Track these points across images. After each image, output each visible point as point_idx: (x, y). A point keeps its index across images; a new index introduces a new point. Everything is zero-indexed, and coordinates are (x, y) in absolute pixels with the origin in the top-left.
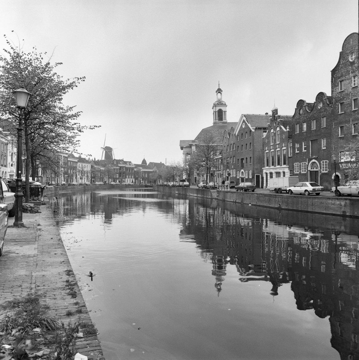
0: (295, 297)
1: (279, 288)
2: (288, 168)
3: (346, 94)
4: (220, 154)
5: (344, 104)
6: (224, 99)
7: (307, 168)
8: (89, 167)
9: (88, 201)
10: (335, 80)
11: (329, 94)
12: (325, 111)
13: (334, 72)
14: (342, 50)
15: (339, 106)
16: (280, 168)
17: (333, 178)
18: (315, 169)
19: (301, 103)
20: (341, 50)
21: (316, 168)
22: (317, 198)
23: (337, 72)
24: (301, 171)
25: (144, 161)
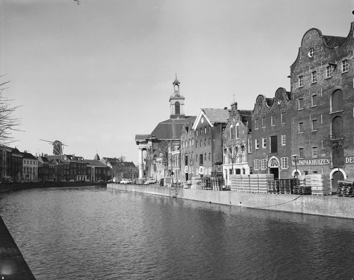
12: (284, 107)
13: (293, 67)
21: (276, 165)
23: (296, 67)
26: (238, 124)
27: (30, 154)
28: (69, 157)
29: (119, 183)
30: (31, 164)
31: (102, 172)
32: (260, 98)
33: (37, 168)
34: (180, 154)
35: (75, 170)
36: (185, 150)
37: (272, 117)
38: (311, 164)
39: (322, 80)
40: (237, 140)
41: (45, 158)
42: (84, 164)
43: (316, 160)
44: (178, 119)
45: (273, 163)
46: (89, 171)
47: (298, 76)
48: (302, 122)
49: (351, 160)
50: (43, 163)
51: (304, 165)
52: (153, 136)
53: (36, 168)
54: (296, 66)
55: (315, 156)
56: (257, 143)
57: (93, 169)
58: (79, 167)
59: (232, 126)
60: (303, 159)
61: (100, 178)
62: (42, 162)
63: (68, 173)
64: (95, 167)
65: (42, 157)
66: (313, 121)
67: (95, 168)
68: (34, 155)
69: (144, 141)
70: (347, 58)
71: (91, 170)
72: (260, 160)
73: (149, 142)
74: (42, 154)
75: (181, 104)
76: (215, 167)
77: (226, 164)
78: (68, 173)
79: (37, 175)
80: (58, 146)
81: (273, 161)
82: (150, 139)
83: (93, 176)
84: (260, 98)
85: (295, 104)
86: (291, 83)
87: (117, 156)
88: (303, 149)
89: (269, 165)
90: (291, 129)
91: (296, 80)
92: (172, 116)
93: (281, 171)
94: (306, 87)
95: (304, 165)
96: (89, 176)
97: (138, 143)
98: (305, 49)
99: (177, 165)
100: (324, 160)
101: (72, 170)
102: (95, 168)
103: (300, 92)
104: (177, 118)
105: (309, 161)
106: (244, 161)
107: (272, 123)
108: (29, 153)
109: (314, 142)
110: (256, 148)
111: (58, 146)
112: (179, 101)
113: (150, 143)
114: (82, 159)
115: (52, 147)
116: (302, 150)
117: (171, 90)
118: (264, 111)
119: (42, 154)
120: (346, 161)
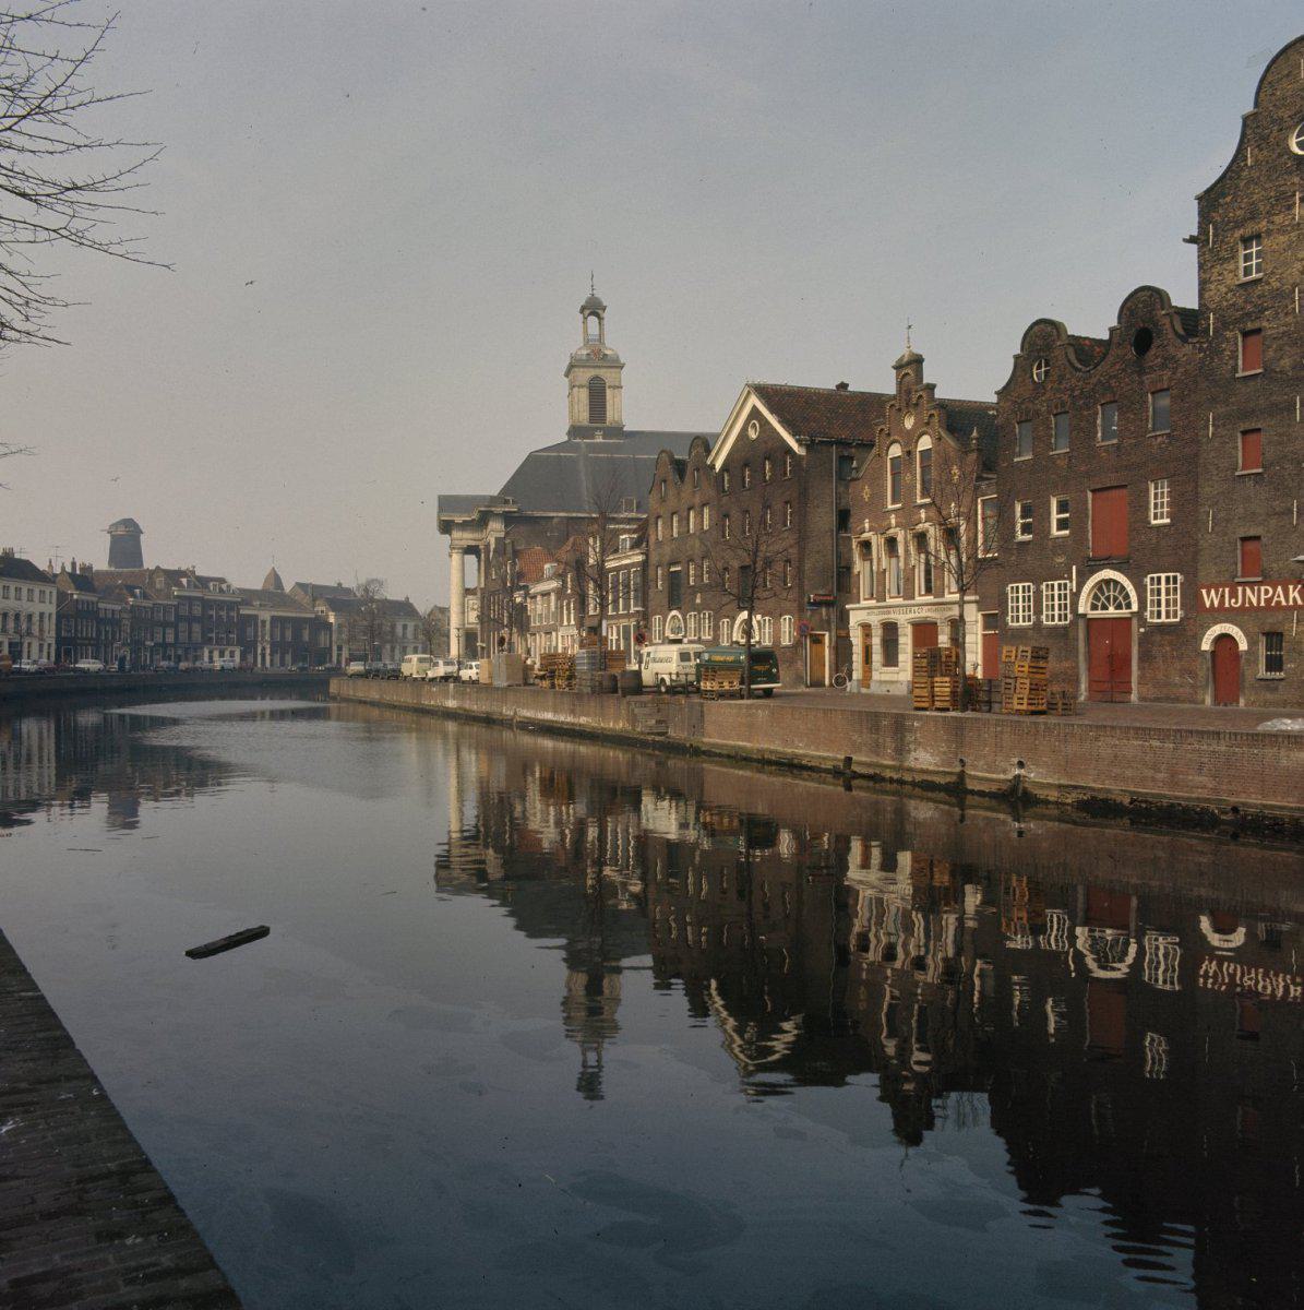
0: (1194, 1262)
1: (1193, 1271)
3: (1271, 291)
4: (636, 545)
5: (1263, 333)
6: (612, 345)
7: (1075, 604)
8: (47, 596)
10: (1215, 235)
11: (1185, 296)
12: (1163, 366)
13: (1209, 201)
14: (1256, 104)
15: (1236, 344)
16: (879, 607)
17: (1206, 645)
18: (1111, 609)
20: (1249, 108)
21: (1119, 607)
23: (1228, 199)
24: (1044, 617)
25: (275, 578)
26: (925, 443)
27: (28, 563)
28: (173, 576)
30: (30, 600)
31: (297, 635)
32: (1043, 340)
33: (54, 617)
34: (645, 565)
35: (197, 628)
36: (667, 550)
37: (1099, 407)
40: (921, 506)
41: (83, 579)
42: (232, 606)
44: (599, 440)
45: (1103, 599)
46: (250, 631)
47: (1238, 233)
48: (1253, 426)
50: (75, 597)
51: (1262, 604)
52: (506, 502)
53: (50, 615)
54: (1224, 195)
56: (1059, 512)
57: (264, 622)
58: (212, 616)
59: (896, 451)
60: (1260, 579)
61: (288, 658)
62: (72, 594)
63: (170, 639)
65: (72, 575)
67: (274, 619)
68: (42, 566)
69: (474, 520)
71: (256, 625)
73: (491, 523)
74: (74, 564)
75: (610, 387)
76: (809, 613)
77: (864, 603)
78: (170, 639)
79: (53, 641)
80: (126, 540)
81: (1100, 589)
82: (499, 510)
83: (264, 649)
84: (1043, 340)
85: (1217, 352)
86: (1201, 266)
87: (349, 577)
88: (1257, 538)
89: (1083, 607)
90: (1196, 455)
91: (1223, 254)
92: (575, 431)
93: (1142, 630)
94: (1279, 280)
95: (1262, 604)
96: (248, 647)
97: (446, 527)
98: (1274, 122)
99: (627, 607)
101: (183, 626)
102: (274, 619)
104: (593, 438)
105: (1291, 587)
106: (892, 595)
107: (1099, 435)
108: (24, 557)
110: (1021, 537)
111: (126, 540)
112: (602, 373)
113: (496, 529)
114: (224, 586)
115: (105, 542)
116: (1251, 546)
117: (571, 337)
118: (1060, 383)
119: (74, 564)
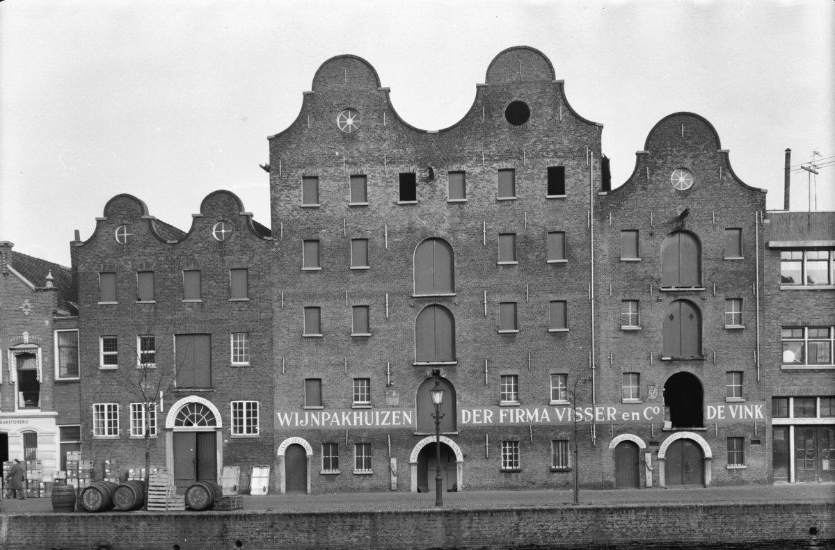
2: (54, 420)
9: (29, 351)
19: (124, 209)
22: (207, 517)
29: (621, 402)
38: (350, 424)
39: (386, 203)
43: (366, 413)
47: (301, 172)
49: (477, 417)
55: (360, 402)
64: (14, 411)
66: (354, 307)
70: (464, 168)
72: (124, 406)
86: (272, 188)
100: (394, 413)
103: (307, 220)
105: (343, 413)
109: (362, 364)
120: (462, 419)
